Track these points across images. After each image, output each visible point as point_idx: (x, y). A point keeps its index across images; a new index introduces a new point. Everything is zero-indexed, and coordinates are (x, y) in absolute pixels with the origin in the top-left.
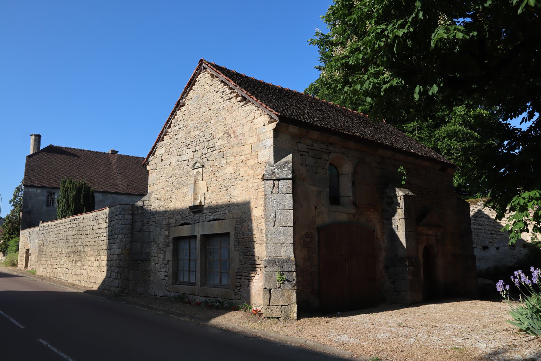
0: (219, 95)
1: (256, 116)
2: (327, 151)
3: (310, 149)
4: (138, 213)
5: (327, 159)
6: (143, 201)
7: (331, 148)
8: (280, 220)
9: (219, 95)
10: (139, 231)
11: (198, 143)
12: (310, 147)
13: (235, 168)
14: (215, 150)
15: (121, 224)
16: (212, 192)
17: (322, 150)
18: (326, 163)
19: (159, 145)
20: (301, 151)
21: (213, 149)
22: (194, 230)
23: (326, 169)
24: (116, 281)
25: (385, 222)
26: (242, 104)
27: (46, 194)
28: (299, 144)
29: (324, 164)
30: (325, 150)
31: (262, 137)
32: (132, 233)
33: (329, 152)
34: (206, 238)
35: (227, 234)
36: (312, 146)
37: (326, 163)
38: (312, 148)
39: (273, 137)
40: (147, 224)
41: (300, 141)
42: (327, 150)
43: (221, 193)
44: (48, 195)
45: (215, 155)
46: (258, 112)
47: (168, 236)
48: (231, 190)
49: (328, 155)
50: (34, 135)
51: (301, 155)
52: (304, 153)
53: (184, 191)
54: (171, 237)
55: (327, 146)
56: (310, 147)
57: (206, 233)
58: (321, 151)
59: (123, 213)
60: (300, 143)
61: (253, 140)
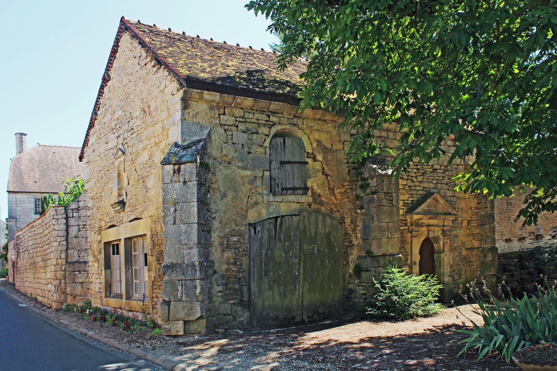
0: (137, 60)
1: (168, 83)
2: (268, 123)
3: (239, 122)
4: (73, 217)
5: (268, 133)
6: (78, 202)
7: (274, 119)
8: (181, 216)
9: (137, 60)
10: (76, 237)
11: (120, 125)
12: (241, 119)
13: (150, 153)
14: (134, 132)
15: (55, 230)
16: (133, 186)
17: (260, 122)
18: (265, 140)
19: (91, 132)
20: (225, 125)
21: (132, 131)
22: (119, 233)
23: (266, 147)
24: (55, 295)
25: (359, 211)
26: (156, 69)
27: (33, 200)
28: (221, 116)
29: (263, 141)
30: (264, 122)
31: (172, 111)
32: (67, 240)
33: (272, 123)
34: (128, 240)
35: (145, 235)
36: (243, 118)
37: (265, 140)
38: (244, 120)
39: (180, 109)
40: (84, 228)
41: (225, 112)
42: (267, 121)
43: (139, 186)
44: (36, 202)
45: (134, 139)
46: (169, 77)
47: (100, 241)
48: (147, 180)
49: (270, 128)
50: (19, 133)
51: (225, 130)
52: (230, 127)
53: (110, 186)
54: (103, 242)
55: (269, 116)
56: (241, 119)
57: (128, 236)
58: (259, 123)
59: (56, 217)
60: (224, 114)
61: (164, 115)
